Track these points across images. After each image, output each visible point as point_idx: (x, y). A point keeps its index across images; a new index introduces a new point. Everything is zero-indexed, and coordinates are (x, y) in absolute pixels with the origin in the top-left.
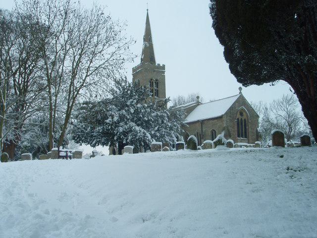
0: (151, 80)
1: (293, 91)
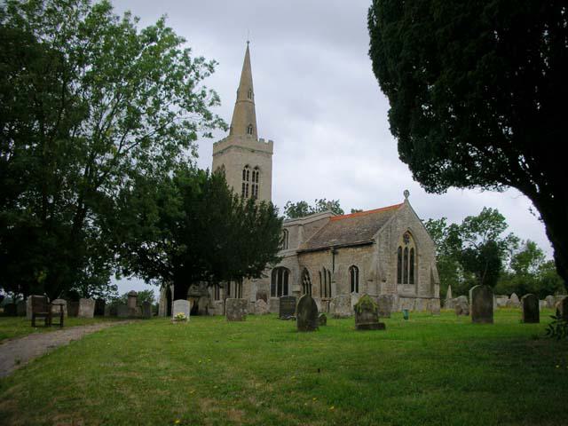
0: (247, 166)
1: (538, 214)
